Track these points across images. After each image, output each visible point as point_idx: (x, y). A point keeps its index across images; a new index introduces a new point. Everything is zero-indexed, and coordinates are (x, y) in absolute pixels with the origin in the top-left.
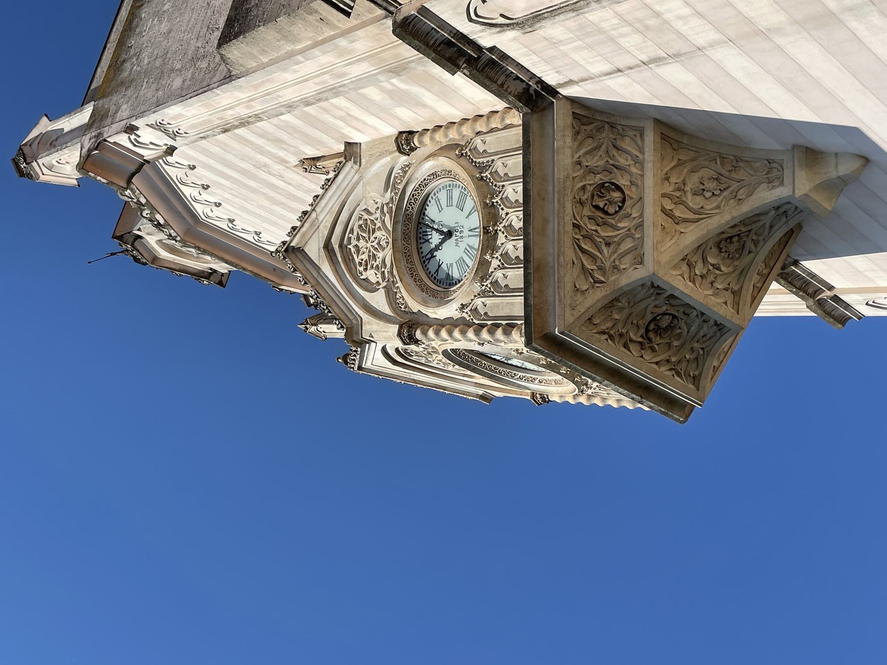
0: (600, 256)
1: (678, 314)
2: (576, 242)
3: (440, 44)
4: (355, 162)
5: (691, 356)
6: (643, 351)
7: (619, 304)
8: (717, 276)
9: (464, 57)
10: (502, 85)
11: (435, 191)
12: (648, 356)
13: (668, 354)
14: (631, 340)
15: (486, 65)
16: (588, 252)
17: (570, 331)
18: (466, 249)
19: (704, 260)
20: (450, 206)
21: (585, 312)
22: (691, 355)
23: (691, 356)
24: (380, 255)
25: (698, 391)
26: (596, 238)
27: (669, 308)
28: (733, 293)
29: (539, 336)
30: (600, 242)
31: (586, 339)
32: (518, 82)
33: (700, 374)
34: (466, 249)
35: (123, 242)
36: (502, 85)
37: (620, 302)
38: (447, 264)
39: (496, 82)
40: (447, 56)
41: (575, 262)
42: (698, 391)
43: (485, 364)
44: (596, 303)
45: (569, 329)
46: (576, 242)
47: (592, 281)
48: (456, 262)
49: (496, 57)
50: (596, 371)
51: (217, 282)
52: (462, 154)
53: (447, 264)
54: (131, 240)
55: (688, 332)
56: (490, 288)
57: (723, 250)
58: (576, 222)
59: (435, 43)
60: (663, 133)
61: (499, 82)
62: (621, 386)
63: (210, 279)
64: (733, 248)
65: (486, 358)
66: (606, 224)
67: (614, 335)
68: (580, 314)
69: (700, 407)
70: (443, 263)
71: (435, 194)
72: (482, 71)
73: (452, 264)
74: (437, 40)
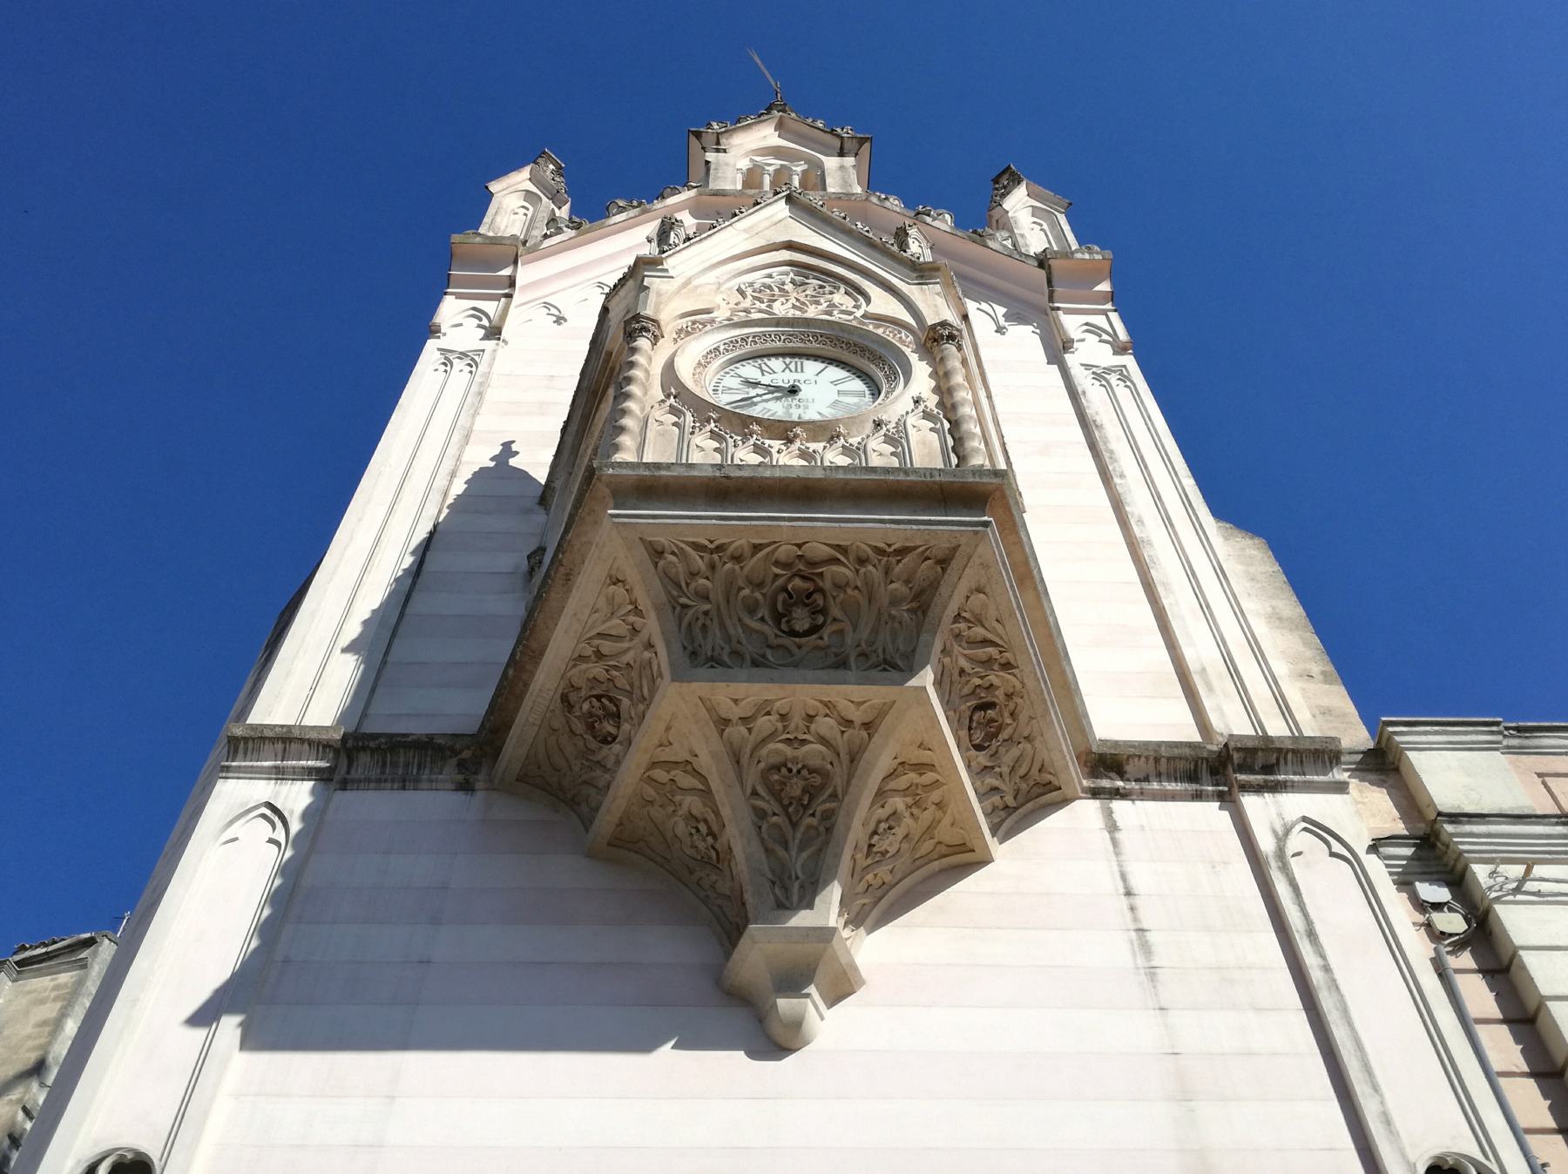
0: (966, 652)
1: (795, 643)
2: (1002, 647)
3: (1278, 760)
5: (695, 584)
6: (799, 553)
7: (908, 607)
8: (784, 731)
9: (1238, 764)
10: (1157, 760)
12: (784, 552)
13: (746, 570)
14: (836, 561)
15: (1195, 770)
16: (980, 645)
17: (976, 533)
19: (823, 741)
21: (964, 570)
22: (696, 587)
23: (695, 584)
25: (640, 539)
26: (980, 670)
27: (820, 642)
28: (727, 722)
29: (992, 496)
30: (973, 669)
31: (937, 534)
32: (1141, 776)
33: (656, 564)
35: (856, 138)
36: (1157, 760)
37: (908, 610)
39: (1169, 759)
40: (1260, 754)
41: (995, 624)
42: (640, 539)
43: (772, 341)
44: (953, 592)
45: (979, 535)
46: (1002, 647)
47: (964, 614)
49: (1207, 791)
50: (946, 512)
51: (704, 135)
54: (847, 145)
55: (740, 620)
57: (805, 772)
58: (1011, 671)
59: (1285, 759)
60: (970, 853)
61: (1163, 761)
62: (781, 480)
63: (715, 135)
64: (795, 788)
65: (781, 351)
66: (970, 694)
67: (880, 558)
68: (969, 565)
69: (1384, 719)
72: (1197, 762)
74: (1286, 763)
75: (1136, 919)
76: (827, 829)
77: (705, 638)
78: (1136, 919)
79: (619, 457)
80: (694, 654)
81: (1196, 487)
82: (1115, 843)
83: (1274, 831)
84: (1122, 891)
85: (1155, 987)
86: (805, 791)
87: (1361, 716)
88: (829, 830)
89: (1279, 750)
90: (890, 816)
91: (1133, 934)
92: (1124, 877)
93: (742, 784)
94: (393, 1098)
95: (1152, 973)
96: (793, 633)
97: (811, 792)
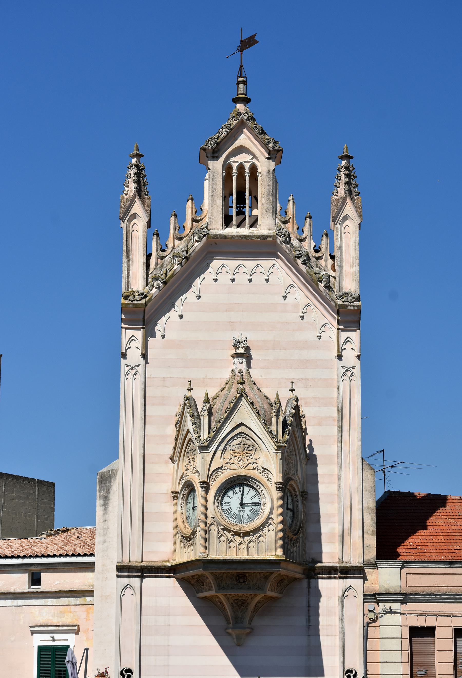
4: (276, 450)
11: (260, 497)
15: (331, 571)
18: (236, 513)
20: (250, 510)
24: (236, 462)
34: (236, 513)
36: (322, 570)
38: (230, 502)
48: (230, 507)
52: (270, 518)
53: (230, 502)
56: (220, 534)
70: (231, 499)
71: (258, 495)
73: (230, 505)
75: (309, 613)
76: (246, 609)
77: (222, 583)
78: (309, 613)
79: (123, 324)
80: (220, 586)
81: (361, 447)
82: (309, 592)
83: (343, 590)
84: (307, 606)
85: (309, 630)
86: (242, 603)
87: (376, 548)
88: (247, 609)
89: (349, 569)
90: (255, 369)
91: (307, 617)
92: (309, 602)
93: (229, 603)
94: (169, 656)
95: (309, 627)
96: (240, 582)
97: (243, 603)
